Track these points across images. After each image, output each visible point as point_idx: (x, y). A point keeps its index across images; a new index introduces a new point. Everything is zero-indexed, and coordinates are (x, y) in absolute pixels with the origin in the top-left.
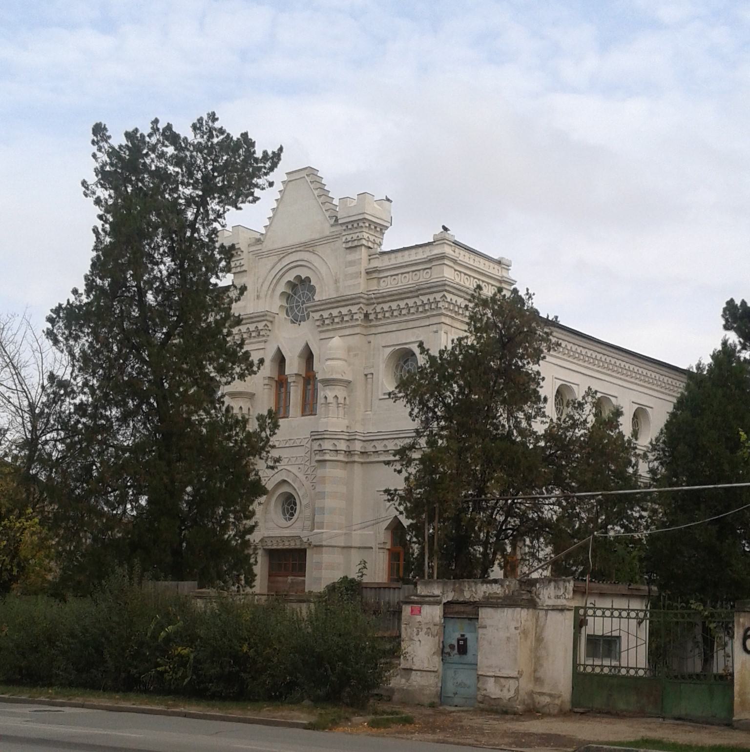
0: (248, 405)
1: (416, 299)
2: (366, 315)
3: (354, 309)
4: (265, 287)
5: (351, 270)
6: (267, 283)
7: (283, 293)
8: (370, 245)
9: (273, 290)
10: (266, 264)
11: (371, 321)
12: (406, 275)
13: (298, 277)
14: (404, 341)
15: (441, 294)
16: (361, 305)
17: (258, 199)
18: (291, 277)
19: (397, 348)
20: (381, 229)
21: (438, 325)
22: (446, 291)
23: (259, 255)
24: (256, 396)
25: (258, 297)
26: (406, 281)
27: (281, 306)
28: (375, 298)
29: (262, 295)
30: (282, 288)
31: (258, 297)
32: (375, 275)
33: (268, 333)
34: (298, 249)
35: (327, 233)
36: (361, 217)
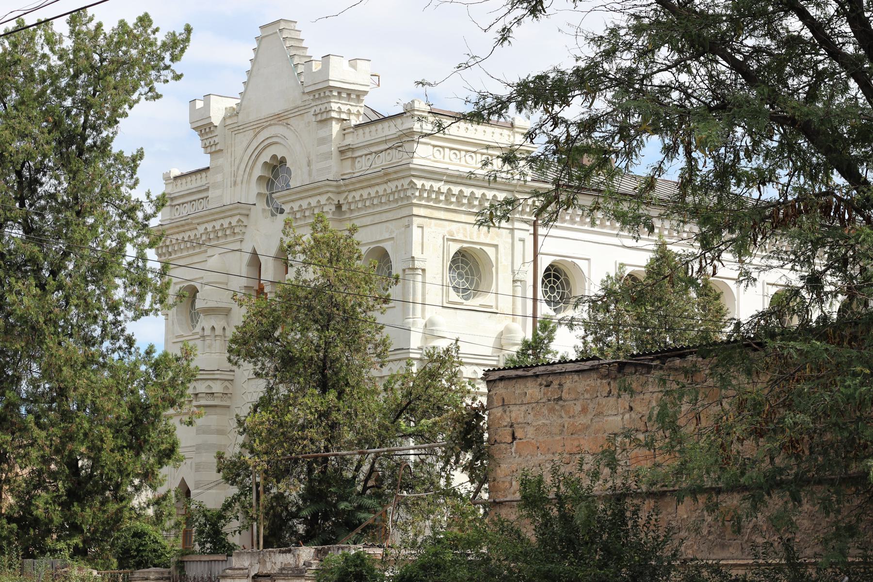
0: (223, 323)
1: (385, 186)
2: (339, 206)
3: (323, 199)
4: (241, 172)
5: (324, 149)
6: (243, 166)
7: (260, 178)
8: (344, 116)
9: (250, 174)
10: (242, 140)
11: (345, 212)
12: (389, 151)
13: (274, 157)
14: (378, 238)
15: (407, 181)
16: (330, 195)
17: (158, 96)
18: (266, 157)
19: (372, 247)
20: (358, 96)
21: (407, 219)
22: (413, 176)
23: (237, 129)
24: (232, 311)
25: (235, 182)
26: (382, 161)
27: (259, 194)
28: (345, 185)
29: (239, 179)
30: (258, 171)
31: (235, 182)
32: (349, 154)
33: (244, 230)
34: (272, 122)
35: (299, 103)
36: (325, 85)
